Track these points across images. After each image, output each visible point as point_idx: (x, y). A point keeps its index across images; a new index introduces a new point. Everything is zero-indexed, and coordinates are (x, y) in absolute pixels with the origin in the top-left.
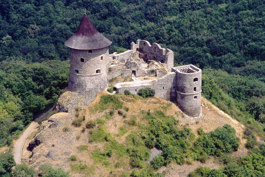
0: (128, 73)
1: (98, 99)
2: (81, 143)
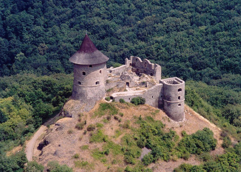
0: (123, 84)
1: (97, 106)
2: (83, 143)
